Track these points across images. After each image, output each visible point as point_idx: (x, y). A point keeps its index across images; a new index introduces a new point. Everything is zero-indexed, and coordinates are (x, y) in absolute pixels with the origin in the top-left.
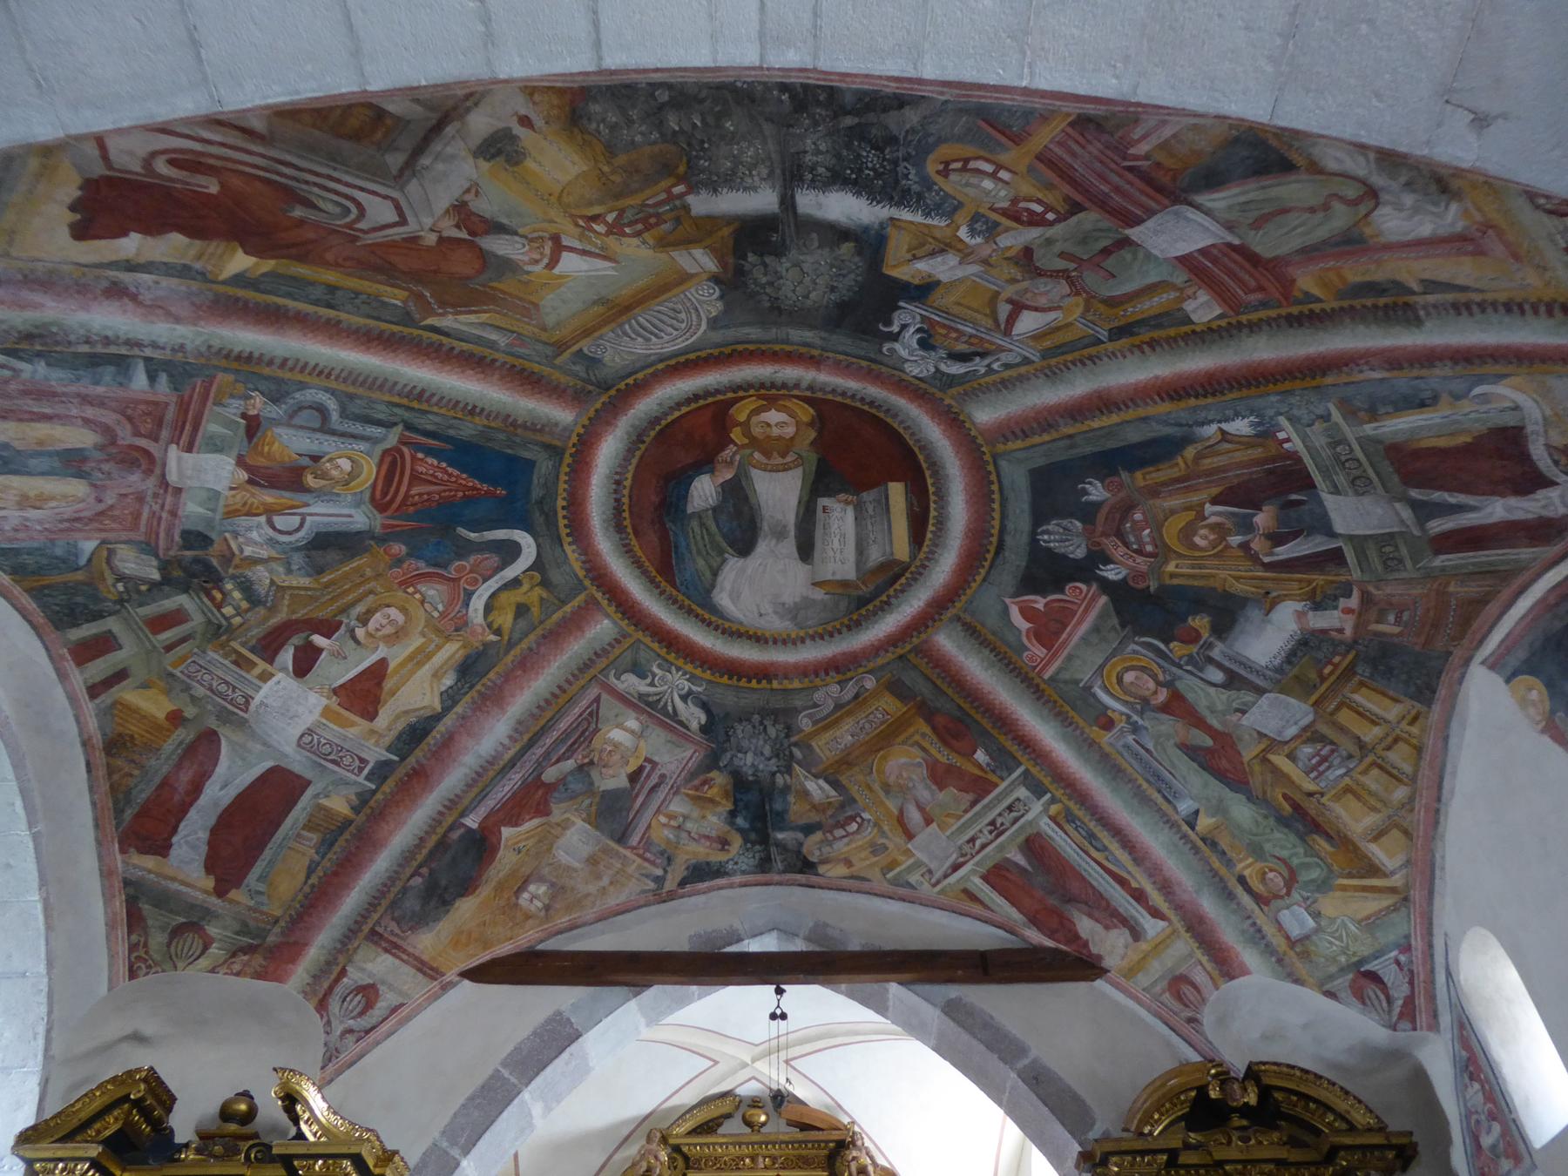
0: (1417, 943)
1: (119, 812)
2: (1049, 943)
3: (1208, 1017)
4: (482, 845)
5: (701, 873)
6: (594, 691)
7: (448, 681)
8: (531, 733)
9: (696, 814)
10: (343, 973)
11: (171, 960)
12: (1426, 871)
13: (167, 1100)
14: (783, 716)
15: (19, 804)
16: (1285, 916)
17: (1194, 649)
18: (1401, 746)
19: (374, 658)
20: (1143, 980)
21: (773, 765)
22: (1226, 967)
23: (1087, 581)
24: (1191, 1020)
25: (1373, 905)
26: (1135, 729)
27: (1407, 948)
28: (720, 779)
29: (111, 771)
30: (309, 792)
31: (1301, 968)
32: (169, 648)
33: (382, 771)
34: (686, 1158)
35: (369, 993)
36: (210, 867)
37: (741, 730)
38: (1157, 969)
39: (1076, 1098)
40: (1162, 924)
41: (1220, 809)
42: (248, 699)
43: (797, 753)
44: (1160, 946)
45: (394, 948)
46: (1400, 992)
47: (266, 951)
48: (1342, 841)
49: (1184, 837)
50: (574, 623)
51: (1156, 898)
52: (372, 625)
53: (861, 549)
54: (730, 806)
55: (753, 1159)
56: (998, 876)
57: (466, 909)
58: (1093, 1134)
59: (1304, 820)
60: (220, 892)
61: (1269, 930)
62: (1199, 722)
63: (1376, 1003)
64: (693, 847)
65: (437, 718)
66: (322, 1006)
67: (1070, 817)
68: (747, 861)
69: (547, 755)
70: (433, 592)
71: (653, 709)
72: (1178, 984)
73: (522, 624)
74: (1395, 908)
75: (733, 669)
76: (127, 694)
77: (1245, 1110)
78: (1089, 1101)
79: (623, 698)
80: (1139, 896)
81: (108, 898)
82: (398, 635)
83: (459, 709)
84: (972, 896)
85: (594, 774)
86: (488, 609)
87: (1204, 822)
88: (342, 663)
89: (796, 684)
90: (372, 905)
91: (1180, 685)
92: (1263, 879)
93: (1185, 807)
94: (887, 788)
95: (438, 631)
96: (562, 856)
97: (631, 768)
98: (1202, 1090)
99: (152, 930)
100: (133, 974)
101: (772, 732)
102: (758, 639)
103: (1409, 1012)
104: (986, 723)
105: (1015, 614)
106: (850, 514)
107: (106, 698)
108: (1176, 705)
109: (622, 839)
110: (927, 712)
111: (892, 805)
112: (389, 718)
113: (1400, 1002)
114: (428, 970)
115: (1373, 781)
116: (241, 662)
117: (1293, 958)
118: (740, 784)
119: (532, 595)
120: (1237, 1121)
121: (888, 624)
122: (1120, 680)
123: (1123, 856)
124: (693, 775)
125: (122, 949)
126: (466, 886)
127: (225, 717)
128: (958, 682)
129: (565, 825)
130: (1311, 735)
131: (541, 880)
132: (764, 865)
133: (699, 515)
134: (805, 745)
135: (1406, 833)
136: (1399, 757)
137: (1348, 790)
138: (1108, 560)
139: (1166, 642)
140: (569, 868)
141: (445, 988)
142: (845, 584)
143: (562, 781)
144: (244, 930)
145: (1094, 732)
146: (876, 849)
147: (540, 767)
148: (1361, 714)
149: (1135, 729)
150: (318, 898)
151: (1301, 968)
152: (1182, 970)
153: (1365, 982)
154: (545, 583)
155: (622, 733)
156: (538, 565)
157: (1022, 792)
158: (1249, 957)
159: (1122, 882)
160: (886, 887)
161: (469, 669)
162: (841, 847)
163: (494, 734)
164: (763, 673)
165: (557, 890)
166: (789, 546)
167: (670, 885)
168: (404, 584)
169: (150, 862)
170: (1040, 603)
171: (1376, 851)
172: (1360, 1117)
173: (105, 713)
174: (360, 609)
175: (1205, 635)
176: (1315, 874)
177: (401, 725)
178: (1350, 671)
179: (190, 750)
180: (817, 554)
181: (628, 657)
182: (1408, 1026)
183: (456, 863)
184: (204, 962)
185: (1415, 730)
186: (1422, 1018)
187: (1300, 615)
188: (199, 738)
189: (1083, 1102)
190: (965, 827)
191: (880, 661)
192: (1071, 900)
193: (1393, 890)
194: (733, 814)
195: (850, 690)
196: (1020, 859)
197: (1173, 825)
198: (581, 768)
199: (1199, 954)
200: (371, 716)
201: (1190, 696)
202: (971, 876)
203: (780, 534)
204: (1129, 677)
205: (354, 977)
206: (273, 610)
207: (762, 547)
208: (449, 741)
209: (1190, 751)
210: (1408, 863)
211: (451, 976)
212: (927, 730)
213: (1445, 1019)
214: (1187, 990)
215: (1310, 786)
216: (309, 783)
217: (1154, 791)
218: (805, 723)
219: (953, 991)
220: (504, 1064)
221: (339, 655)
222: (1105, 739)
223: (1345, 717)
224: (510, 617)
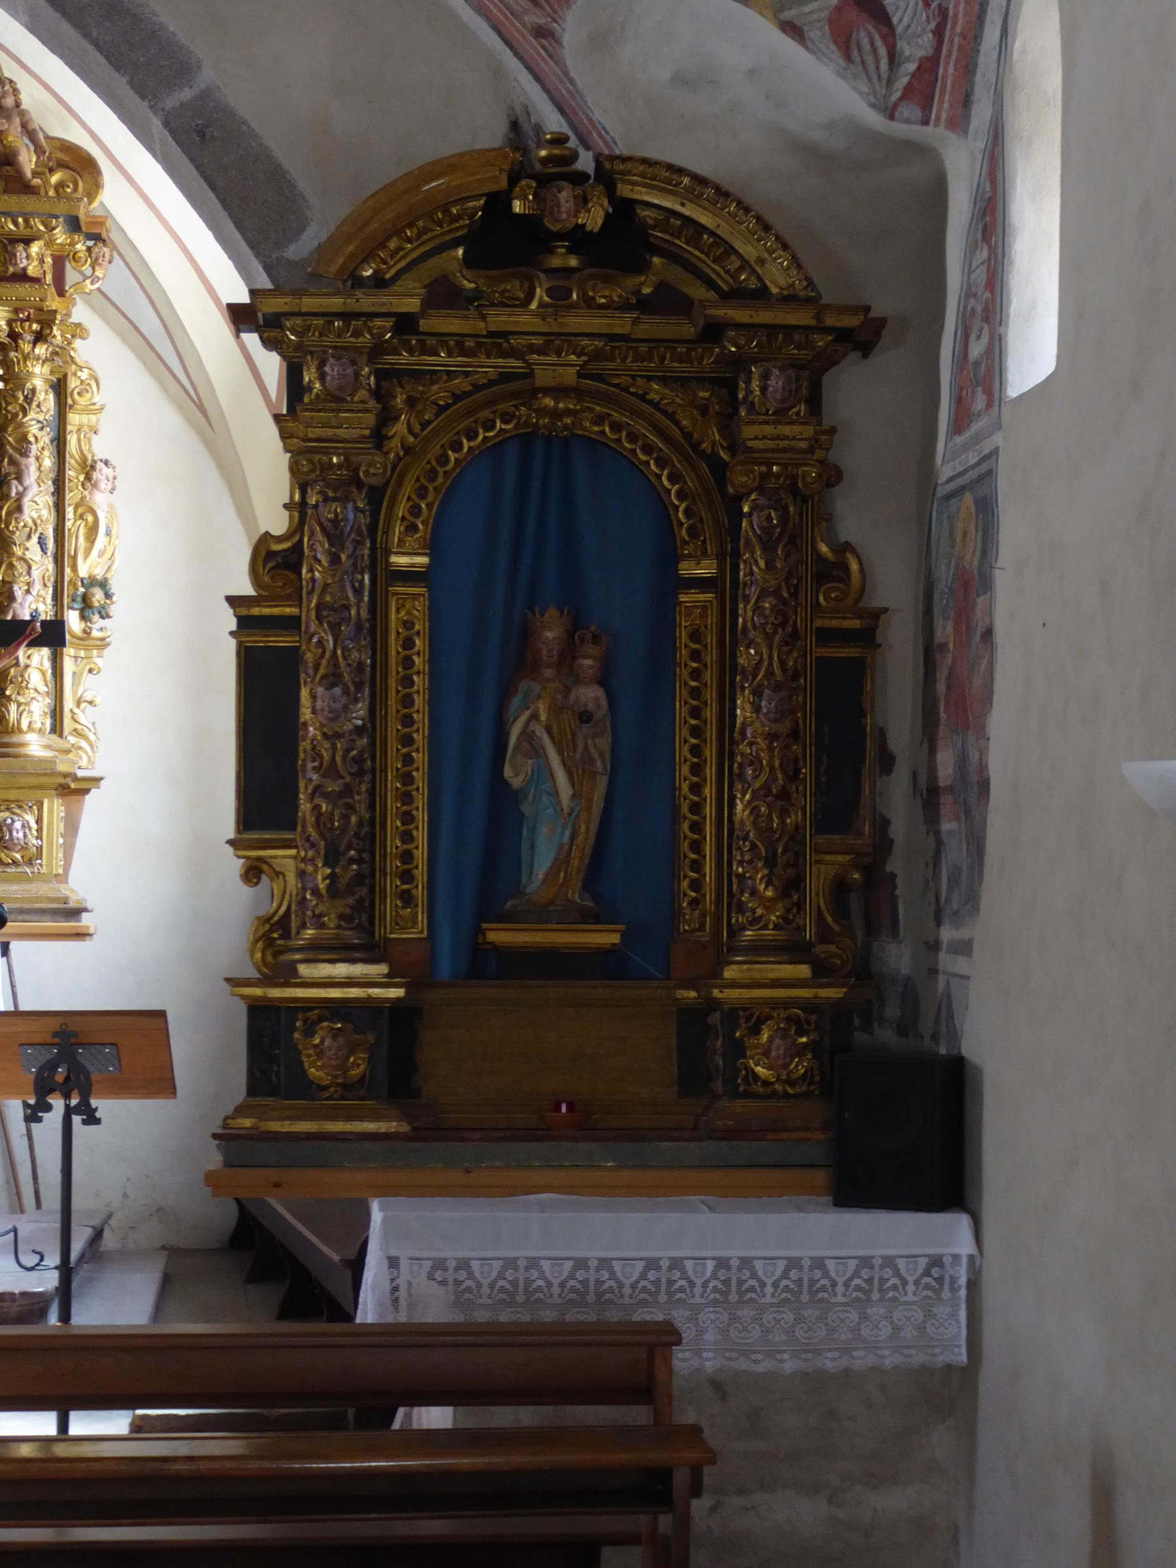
24: (541, 33)
39: (277, 177)
46: (915, 47)
63: (870, 59)
77: (578, 239)
78: (302, 184)
103: (923, 89)
113: (911, 67)
172: (777, 275)
182: (918, 113)
186: (943, 105)
189: (291, 185)
213: (981, 114)
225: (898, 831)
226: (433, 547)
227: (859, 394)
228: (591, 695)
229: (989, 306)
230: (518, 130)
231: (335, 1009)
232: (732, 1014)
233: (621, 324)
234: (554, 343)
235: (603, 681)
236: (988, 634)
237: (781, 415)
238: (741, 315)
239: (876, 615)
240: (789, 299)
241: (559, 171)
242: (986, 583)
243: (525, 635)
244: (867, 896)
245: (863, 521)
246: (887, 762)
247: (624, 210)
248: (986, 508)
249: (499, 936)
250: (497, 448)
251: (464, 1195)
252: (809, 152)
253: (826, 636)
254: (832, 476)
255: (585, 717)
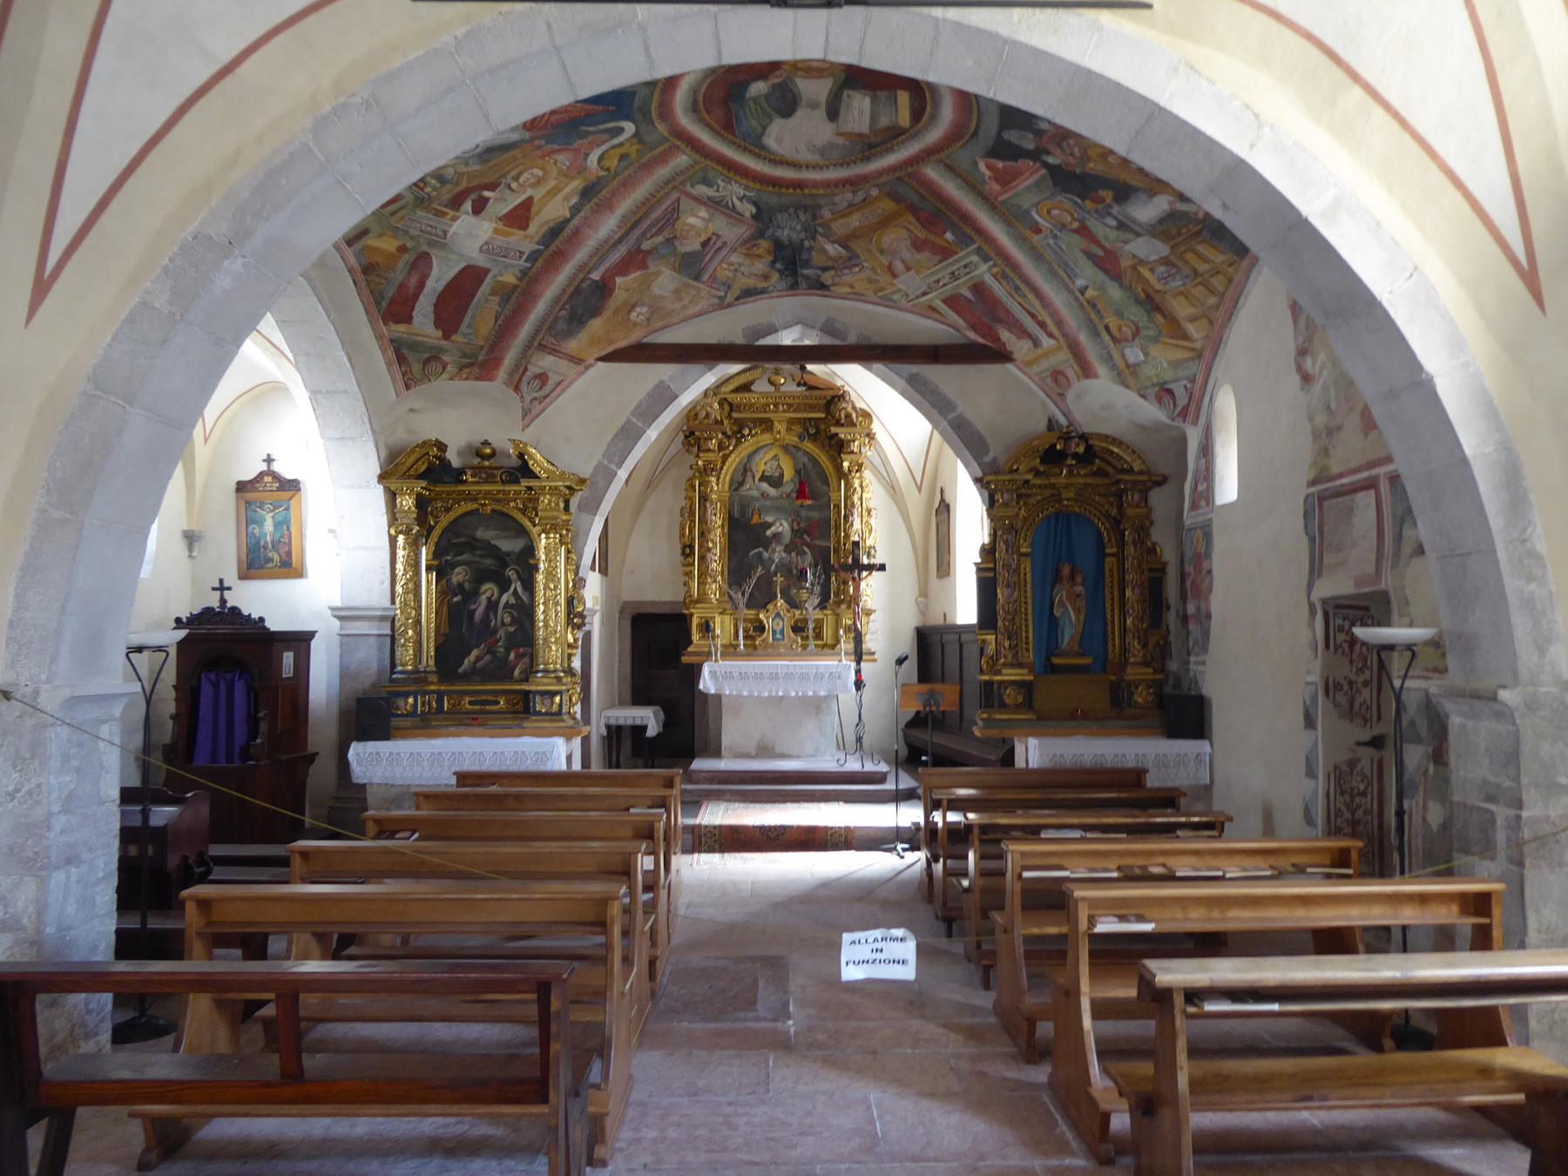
0: (1200, 380)
1: (378, 303)
2: (980, 340)
3: (1070, 395)
4: (603, 289)
5: (749, 293)
6: (675, 195)
7: (574, 200)
8: (632, 223)
9: (747, 262)
10: (526, 369)
11: (426, 378)
12: (1216, 343)
13: (442, 447)
14: (813, 210)
15: (320, 308)
16: (1128, 351)
17: (1100, 207)
18: (1221, 277)
19: (524, 196)
20: (1036, 369)
21: (803, 235)
22: (1086, 371)
23: (1034, 161)
25: (1180, 355)
26: (1055, 237)
27: (1193, 381)
28: (764, 244)
29: (368, 283)
30: (490, 276)
31: (1131, 380)
32: (393, 214)
33: (534, 256)
34: (731, 405)
35: (542, 378)
36: (437, 325)
37: (780, 218)
38: (1045, 365)
39: (982, 440)
40: (1053, 342)
41: (1101, 288)
42: (445, 233)
43: (820, 230)
44: (1048, 354)
45: (553, 351)
46: (1182, 402)
47: (481, 365)
48: (1172, 320)
49: (1076, 299)
50: (663, 158)
51: (1052, 327)
52: (521, 180)
53: (874, 118)
54: (771, 258)
55: (776, 405)
56: (953, 301)
57: (595, 325)
58: (988, 459)
59: (1152, 304)
60: (446, 336)
61: (1117, 357)
62: (1094, 240)
64: (745, 280)
65: (568, 221)
66: (517, 389)
67: (1004, 276)
68: (783, 285)
69: (644, 234)
70: (563, 159)
71: (718, 205)
72: (1057, 375)
73: (624, 163)
74: (1192, 359)
75: (776, 183)
76: (370, 241)
77: (1075, 456)
79: (696, 199)
80: (1042, 325)
81: (384, 352)
82: (539, 182)
83: (582, 214)
84: (934, 309)
85: (677, 243)
86: (600, 159)
87: (1090, 293)
88: (502, 203)
89: (821, 191)
90: (538, 331)
91: (1088, 223)
92: (1120, 328)
93: (1080, 282)
94: (882, 251)
95: (566, 176)
96: (657, 291)
97: (703, 238)
98: (1053, 446)
99: (412, 364)
100: (408, 387)
101: (803, 218)
102: (795, 165)
104: (955, 218)
105: (982, 166)
106: (867, 101)
107: (358, 246)
108: (1083, 231)
109: (697, 278)
110: (913, 209)
111: (884, 260)
112: (536, 227)
114: (575, 360)
115: (1199, 291)
116: (438, 214)
117: (1126, 375)
118: (778, 245)
119: (632, 150)
120: (1071, 462)
121: (891, 159)
122: (1049, 212)
123: (1036, 303)
124: (746, 242)
125: (399, 376)
126: (595, 312)
127: (432, 244)
128: (938, 194)
129: (658, 274)
130: (1165, 261)
131: (644, 304)
132: (794, 286)
133: (755, 100)
134: (826, 226)
135: (1211, 322)
136: (1218, 282)
137: (1181, 293)
138: (1049, 153)
139: (1083, 199)
140: (662, 298)
141: (587, 368)
142: (860, 135)
143: (655, 248)
144: (465, 355)
145: (1028, 233)
146: (870, 281)
147: (639, 241)
148: (1198, 255)
149: (1055, 237)
150: (505, 331)
151: (1131, 380)
152: (1061, 368)
153: (1164, 393)
154: (641, 141)
155: (696, 220)
156: (637, 134)
157: (975, 258)
158: (1101, 369)
159: (1033, 316)
160: (876, 299)
161: (587, 193)
162: (847, 278)
163: (609, 224)
164: (798, 185)
165: (654, 310)
166: (821, 113)
167: (729, 299)
168: (543, 157)
169: (402, 328)
170: (1000, 165)
171: (1191, 328)
173: (358, 255)
174: (514, 173)
175: (1109, 200)
176: (1151, 333)
177: (544, 229)
178: (1199, 233)
179: (414, 266)
180: (842, 114)
181: (701, 174)
183: (588, 300)
184: (444, 376)
185: (1231, 270)
186: (1190, 418)
187: (1170, 203)
188: (418, 258)
190: (933, 274)
191: (882, 180)
192: (999, 321)
193: (1193, 349)
194: (773, 262)
195: (860, 196)
196: (969, 294)
197: (1070, 291)
198: (668, 240)
199: (1072, 361)
200: (524, 227)
201: (1094, 230)
202: (935, 298)
203: (814, 106)
204: (1054, 212)
205: (533, 370)
206: (457, 184)
207: (800, 113)
208: (576, 232)
209: (1089, 255)
210: (1207, 337)
211: (590, 361)
212: (913, 219)
213: (1202, 420)
214: (1061, 379)
215: (1158, 286)
216: (487, 271)
217: (1062, 272)
218: (826, 214)
219: (914, 369)
220: (634, 413)
221: (501, 199)
222: (1035, 238)
223: (1189, 256)
224: (615, 162)
225: (1172, 628)
226: (1032, 545)
227: (1158, 498)
228: (1079, 589)
229: (1207, 474)
230: (1051, 425)
231: (1013, 683)
232: (1129, 684)
233: (1090, 480)
234: (1067, 487)
235: (1083, 584)
236: (1210, 572)
237: (1138, 506)
238: (1126, 477)
239: (1165, 564)
240: (1141, 473)
241: (1066, 437)
242: (1208, 555)
243: (1058, 572)
244: (1164, 651)
245: (1161, 537)
246: (1168, 607)
247: (1089, 448)
248: (1208, 536)
249: (1055, 661)
250: (1048, 518)
251: (784, 802)
252: (1142, 428)
253: (1150, 570)
254: (1152, 523)
255: (1079, 595)
